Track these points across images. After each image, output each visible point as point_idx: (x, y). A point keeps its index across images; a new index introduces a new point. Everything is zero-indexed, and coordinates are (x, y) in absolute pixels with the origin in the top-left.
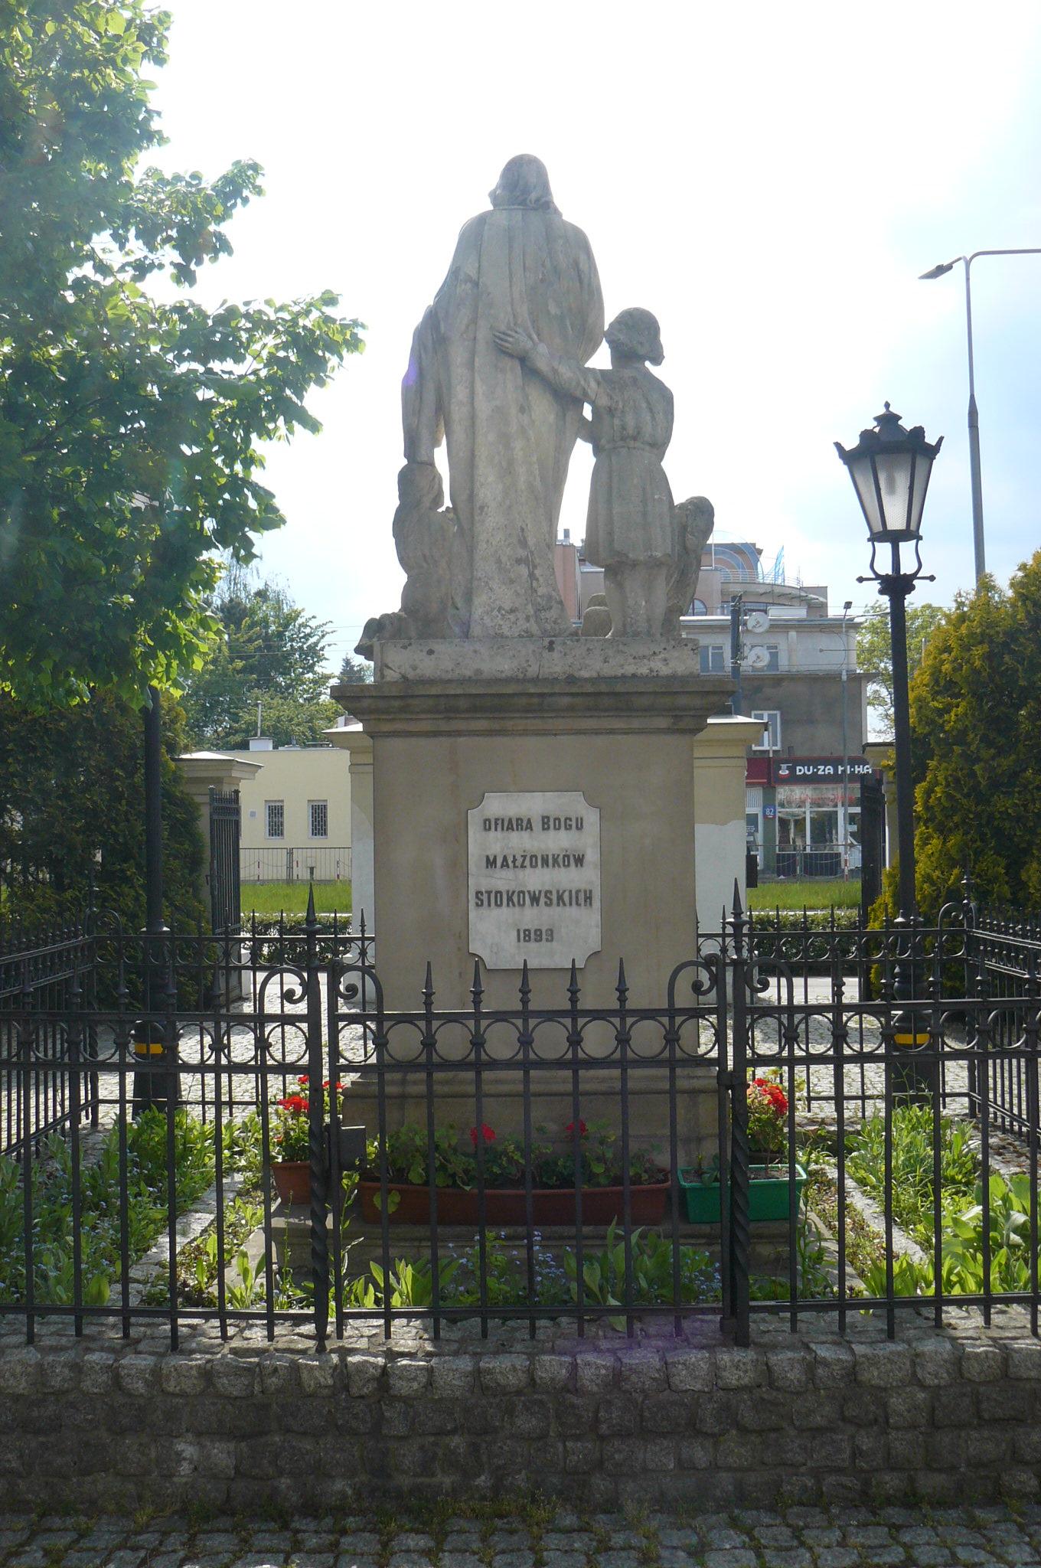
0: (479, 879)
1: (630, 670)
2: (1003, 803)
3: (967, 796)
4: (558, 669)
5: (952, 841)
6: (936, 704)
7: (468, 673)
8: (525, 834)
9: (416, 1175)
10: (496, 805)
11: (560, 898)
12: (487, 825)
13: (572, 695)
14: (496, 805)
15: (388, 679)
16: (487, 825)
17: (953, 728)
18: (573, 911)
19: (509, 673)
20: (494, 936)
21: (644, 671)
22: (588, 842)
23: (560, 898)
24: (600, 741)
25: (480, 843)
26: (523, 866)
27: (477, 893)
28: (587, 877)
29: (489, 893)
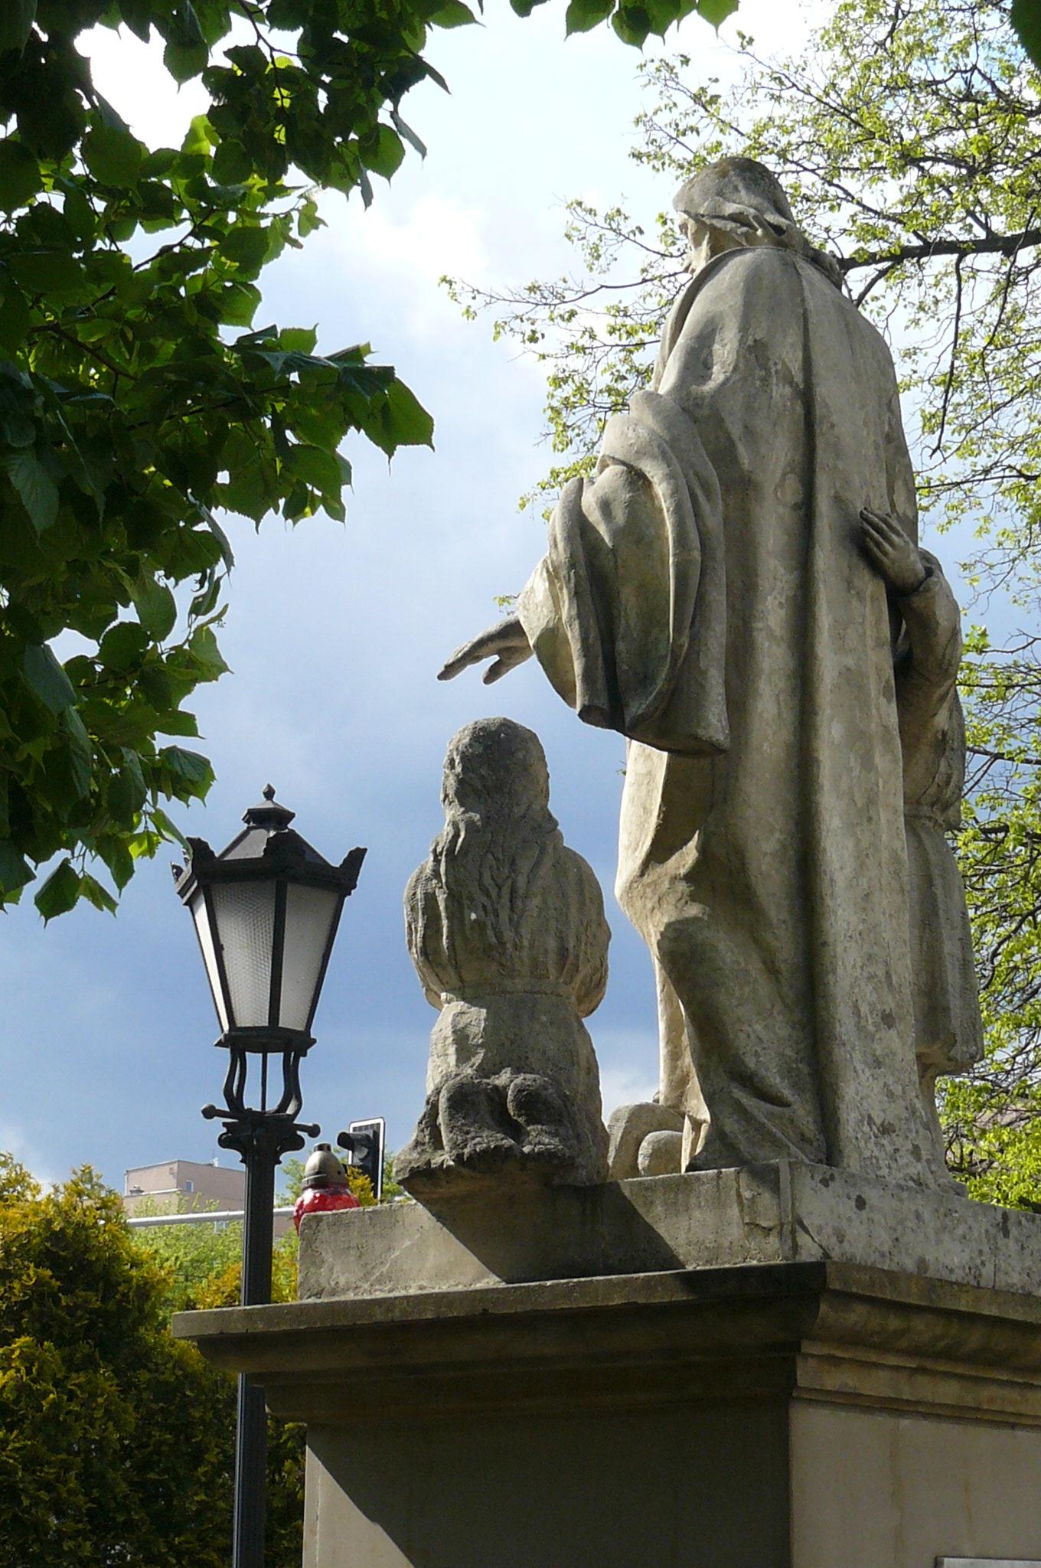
7: (910, 1265)
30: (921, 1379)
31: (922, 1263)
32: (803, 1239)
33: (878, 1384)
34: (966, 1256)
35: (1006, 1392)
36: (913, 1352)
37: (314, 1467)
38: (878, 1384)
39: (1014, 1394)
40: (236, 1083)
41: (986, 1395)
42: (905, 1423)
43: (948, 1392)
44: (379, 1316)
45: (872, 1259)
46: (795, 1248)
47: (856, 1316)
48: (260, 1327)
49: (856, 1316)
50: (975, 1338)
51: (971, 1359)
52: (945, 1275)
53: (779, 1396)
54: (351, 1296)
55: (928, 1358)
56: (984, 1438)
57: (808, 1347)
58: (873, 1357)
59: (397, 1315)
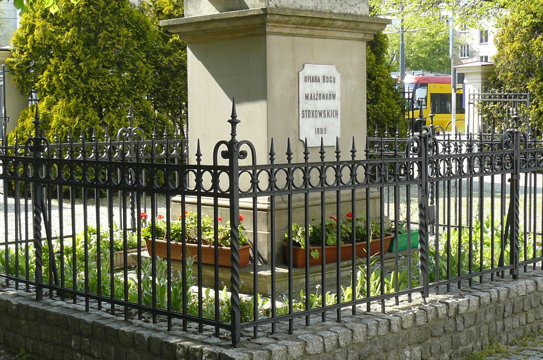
0: (305, 105)
1: (349, 11)
2: (94, 83)
3: (77, 79)
4: (327, 8)
5: (73, 101)
6: (51, 29)
7: (298, 7)
8: (317, 84)
9: (331, 240)
10: (310, 70)
11: (320, 114)
12: (306, 79)
13: (343, 21)
14: (310, 70)
15: (270, 6)
16: (306, 79)
17: (65, 43)
18: (332, 119)
19: (311, 8)
20: (308, 130)
21: (353, 12)
22: (335, 88)
23: (320, 114)
24: (340, 42)
25: (305, 88)
26: (317, 99)
27: (303, 111)
28: (334, 105)
29: (306, 111)
30: (298, 29)
31: (301, 6)
32: (270, 3)
33: (287, 30)
34: (313, 4)
35: (322, 31)
36: (294, 24)
37: (190, 53)
38: (287, 30)
39: (324, 32)
40: (19, 236)
41: (315, 32)
42: (296, 38)
43: (306, 32)
44: (195, 20)
45: (288, 6)
46: (268, 4)
47: (277, 18)
48: (175, 23)
49: (277, 18)
50: (308, 21)
51: (309, 25)
52: (308, 8)
53: (264, 34)
54: (193, 16)
55: (298, 25)
56: (317, 41)
57: (267, 24)
58: (285, 25)
59: (198, 20)
